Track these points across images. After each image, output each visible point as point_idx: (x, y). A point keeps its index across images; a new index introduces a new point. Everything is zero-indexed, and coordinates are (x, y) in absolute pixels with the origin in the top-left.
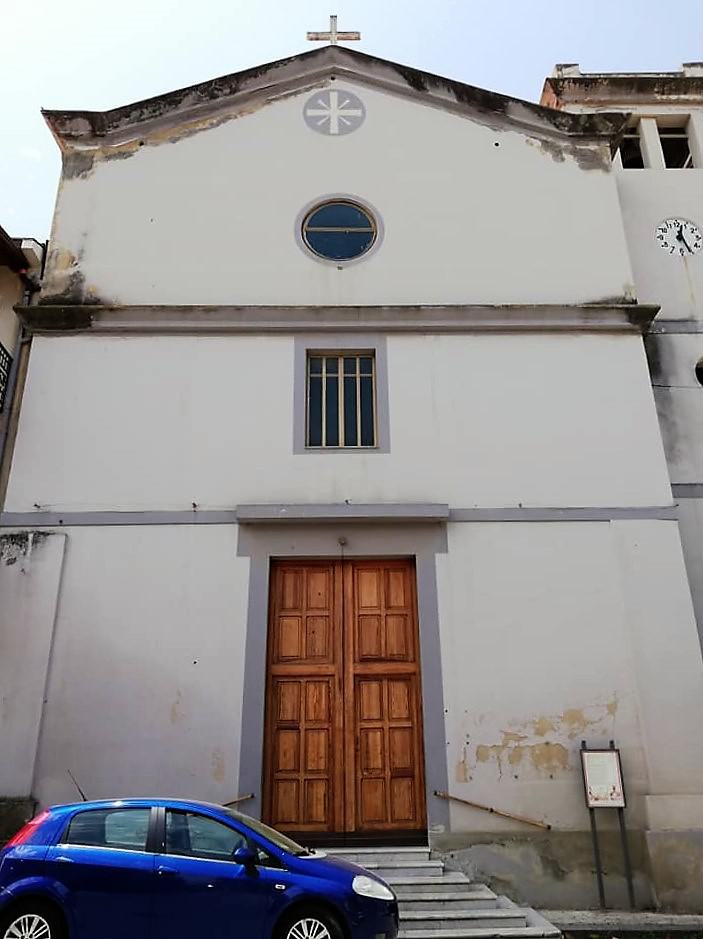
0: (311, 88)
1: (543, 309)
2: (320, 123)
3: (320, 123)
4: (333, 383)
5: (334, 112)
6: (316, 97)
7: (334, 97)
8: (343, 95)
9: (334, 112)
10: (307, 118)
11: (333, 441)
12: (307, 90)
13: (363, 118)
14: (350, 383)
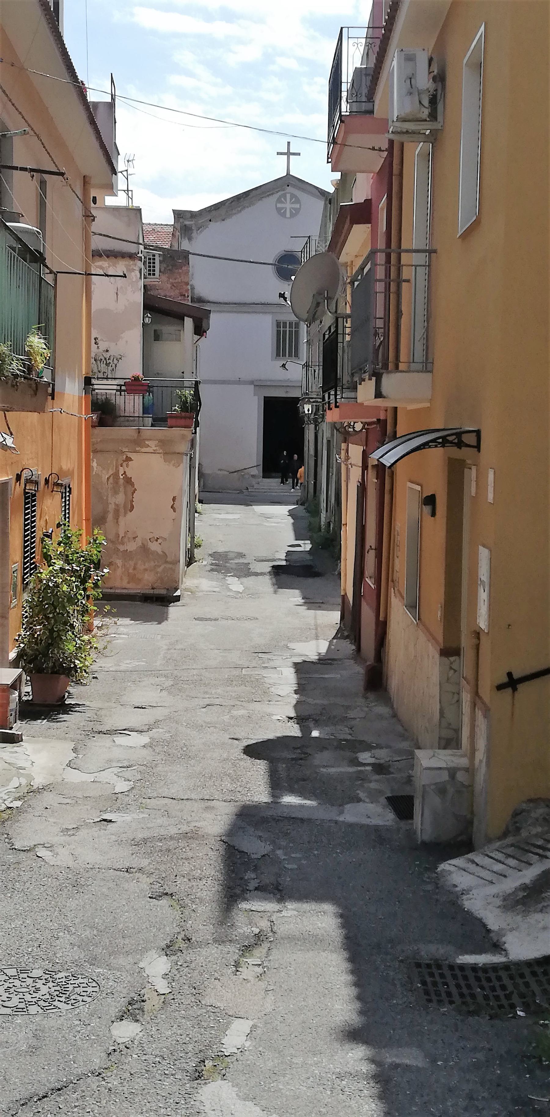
0: (279, 191)
1: (385, 310)
2: (283, 199)
3: (283, 199)
4: (285, 332)
5: (288, 206)
6: (280, 197)
7: (288, 196)
8: (293, 196)
9: (288, 206)
10: (277, 208)
11: (284, 355)
12: (277, 192)
13: (300, 209)
14: (291, 332)
